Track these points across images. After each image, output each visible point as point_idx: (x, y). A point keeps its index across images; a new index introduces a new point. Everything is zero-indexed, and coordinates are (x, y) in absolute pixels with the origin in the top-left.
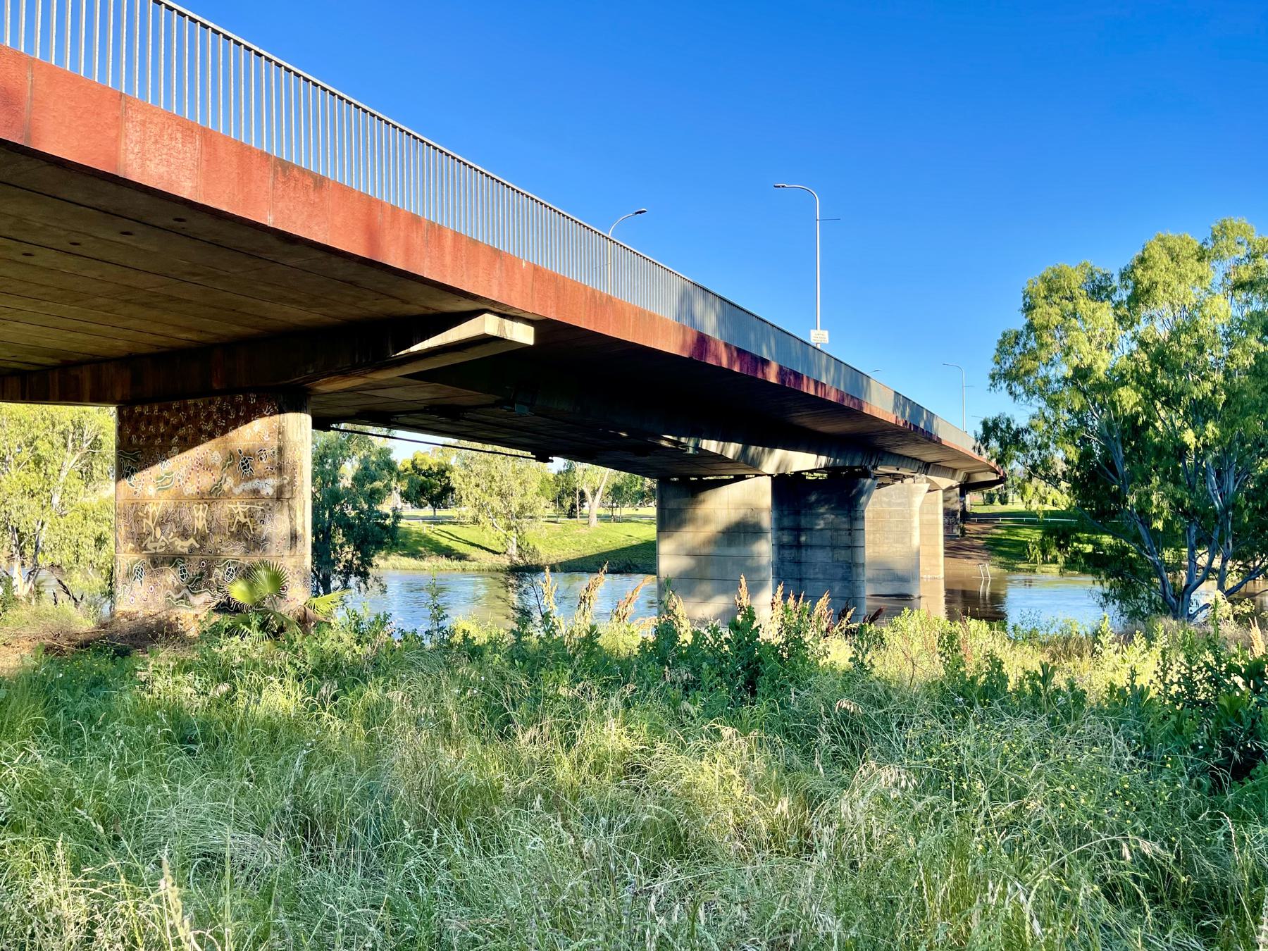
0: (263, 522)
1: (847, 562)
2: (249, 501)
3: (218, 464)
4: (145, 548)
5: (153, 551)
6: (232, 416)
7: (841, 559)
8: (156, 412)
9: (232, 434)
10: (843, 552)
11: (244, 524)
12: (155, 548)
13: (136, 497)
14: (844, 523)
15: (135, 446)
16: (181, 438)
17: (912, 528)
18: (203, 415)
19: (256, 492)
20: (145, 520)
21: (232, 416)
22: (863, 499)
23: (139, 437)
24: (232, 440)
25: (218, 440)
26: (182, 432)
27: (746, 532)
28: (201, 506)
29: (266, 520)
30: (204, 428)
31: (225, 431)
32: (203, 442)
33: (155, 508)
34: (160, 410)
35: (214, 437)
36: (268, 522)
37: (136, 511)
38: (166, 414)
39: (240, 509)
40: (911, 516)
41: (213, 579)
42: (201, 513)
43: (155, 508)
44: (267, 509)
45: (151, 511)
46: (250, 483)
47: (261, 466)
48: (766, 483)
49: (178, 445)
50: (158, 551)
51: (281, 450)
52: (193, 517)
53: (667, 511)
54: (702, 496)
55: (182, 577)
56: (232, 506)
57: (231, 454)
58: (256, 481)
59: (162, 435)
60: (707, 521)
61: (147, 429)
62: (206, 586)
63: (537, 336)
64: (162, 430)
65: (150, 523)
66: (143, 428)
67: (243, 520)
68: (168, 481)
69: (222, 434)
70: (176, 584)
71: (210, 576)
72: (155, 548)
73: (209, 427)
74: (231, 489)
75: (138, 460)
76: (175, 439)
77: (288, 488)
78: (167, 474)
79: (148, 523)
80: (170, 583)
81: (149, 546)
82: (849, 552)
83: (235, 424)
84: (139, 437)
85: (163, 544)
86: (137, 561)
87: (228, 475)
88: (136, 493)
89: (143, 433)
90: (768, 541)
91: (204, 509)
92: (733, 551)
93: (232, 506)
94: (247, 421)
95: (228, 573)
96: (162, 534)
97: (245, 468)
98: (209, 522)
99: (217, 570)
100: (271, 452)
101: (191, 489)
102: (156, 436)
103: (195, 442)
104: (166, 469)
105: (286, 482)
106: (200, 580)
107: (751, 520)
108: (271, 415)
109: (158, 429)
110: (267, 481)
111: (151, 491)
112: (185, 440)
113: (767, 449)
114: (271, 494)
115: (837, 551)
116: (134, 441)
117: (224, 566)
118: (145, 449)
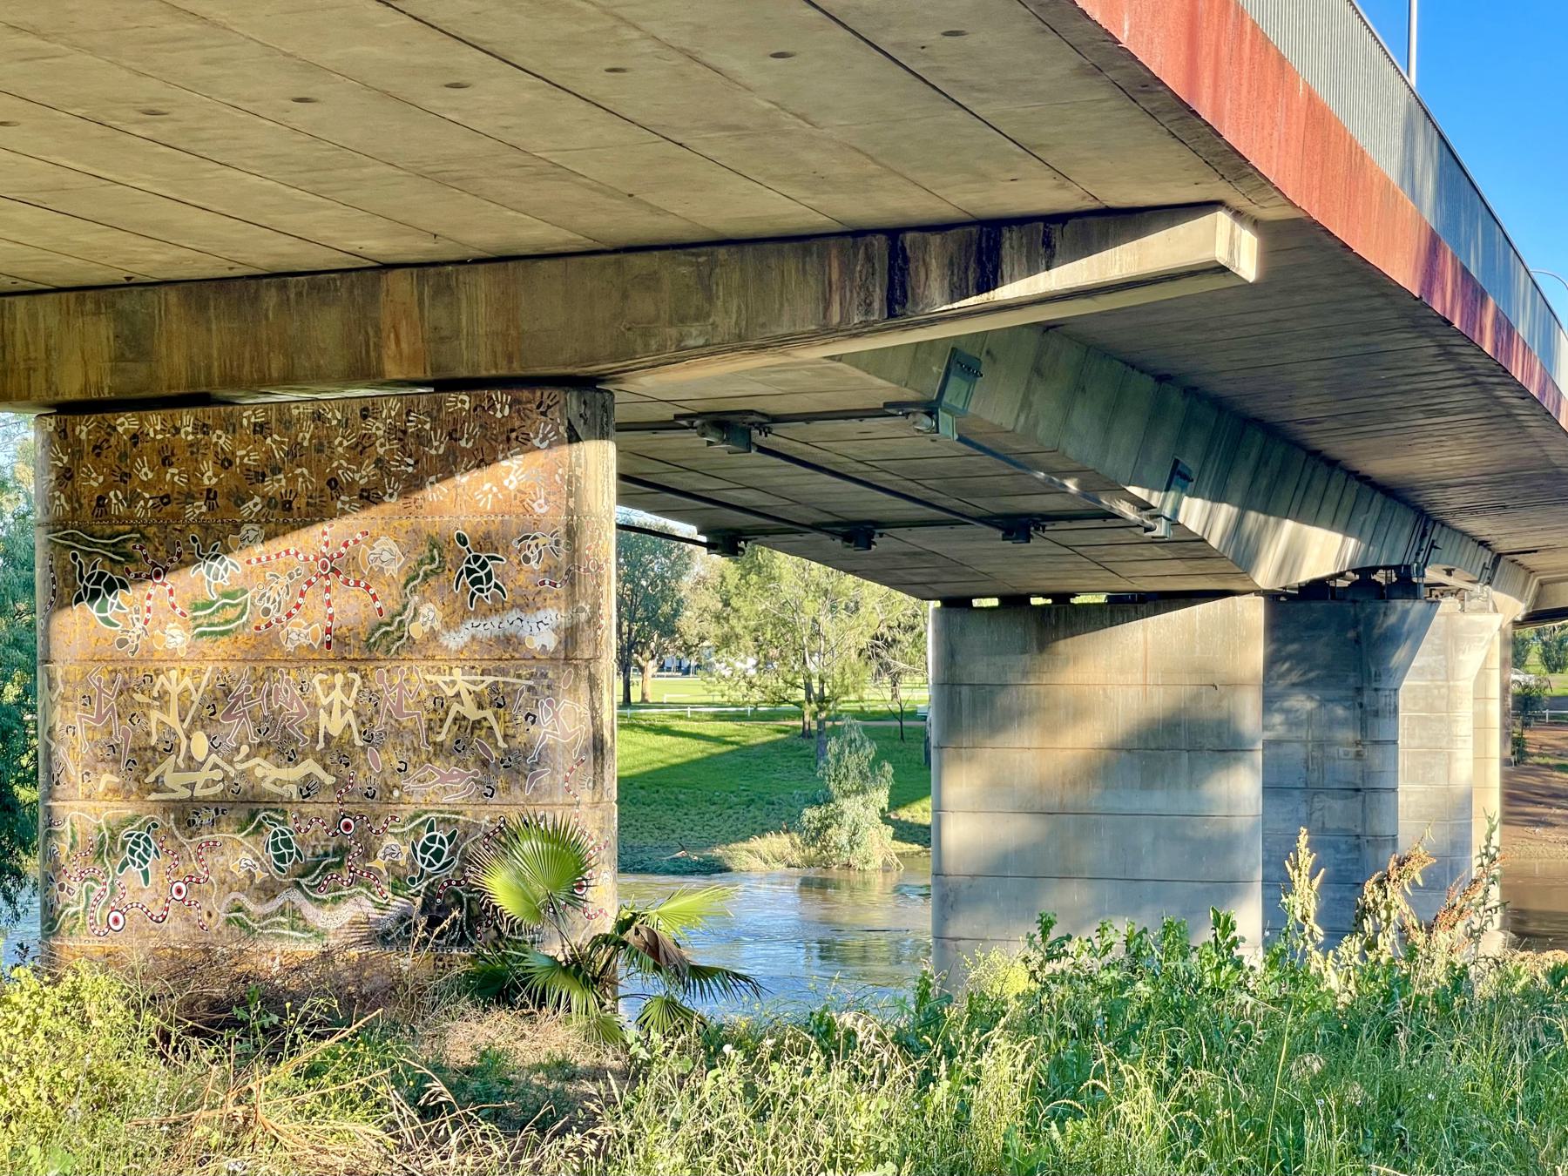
0: (532, 718)
1: (1346, 833)
2: (492, 665)
3: (392, 570)
4: (158, 786)
5: (187, 793)
6: (438, 447)
7: (1331, 825)
8: (187, 433)
9: (436, 493)
10: (1338, 805)
11: (477, 724)
12: (192, 786)
13: (120, 652)
14: (1343, 723)
15: (121, 520)
16: (270, 502)
17: (1452, 738)
18: (341, 444)
19: (509, 641)
20: (155, 715)
21: (438, 447)
22: (1399, 656)
23: (132, 499)
24: (437, 510)
25: (392, 504)
26: (275, 486)
27: (1194, 749)
28: (339, 679)
29: (540, 713)
30: (344, 477)
31: (414, 484)
32: (344, 513)
33: (187, 681)
34: (204, 428)
35: (378, 500)
36: (544, 718)
37: (126, 689)
38: (221, 439)
39: (462, 686)
40: (1451, 706)
41: (379, 863)
42: (337, 695)
43: (187, 681)
44: (541, 690)
45: (174, 690)
46: (496, 620)
47: (516, 574)
48: (1253, 611)
49: (259, 520)
50: (199, 792)
51: (571, 533)
52: (314, 706)
53: (965, 691)
54: (1065, 646)
55: (281, 858)
56: (438, 679)
57: (434, 545)
58: (513, 615)
59: (210, 494)
60: (1078, 712)
61: (160, 478)
62: (355, 881)
63: (1268, 254)
64: (208, 481)
65: (172, 719)
66: (145, 473)
67: (473, 714)
68: (231, 613)
69: (405, 494)
70: (260, 876)
71: (368, 854)
72: (192, 786)
73: (365, 474)
74: (433, 635)
75: (129, 557)
76: (254, 505)
77: (588, 633)
78: (226, 595)
79: (161, 721)
80: (241, 874)
81: (170, 780)
82: (1355, 804)
83: (447, 467)
84: (132, 499)
85: (217, 774)
86: (131, 821)
87: (424, 600)
88: (122, 643)
89: (146, 485)
90: (1253, 767)
91: (348, 685)
92: (1158, 800)
93: (438, 679)
94: (483, 460)
95: (425, 849)
96: (213, 749)
97: (478, 581)
98: (365, 721)
99: (389, 841)
100: (550, 540)
101: (302, 632)
102: (190, 497)
103: (318, 512)
104: (225, 583)
105: (583, 617)
106: (339, 865)
107: (1206, 709)
108: (550, 447)
109: (194, 474)
110: (541, 615)
111: (176, 637)
112: (287, 506)
113: (1272, 519)
114: (551, 645)
115: (1319, 802)
116: (117, 506)
117: (415, 831)
118: (152, 530)
